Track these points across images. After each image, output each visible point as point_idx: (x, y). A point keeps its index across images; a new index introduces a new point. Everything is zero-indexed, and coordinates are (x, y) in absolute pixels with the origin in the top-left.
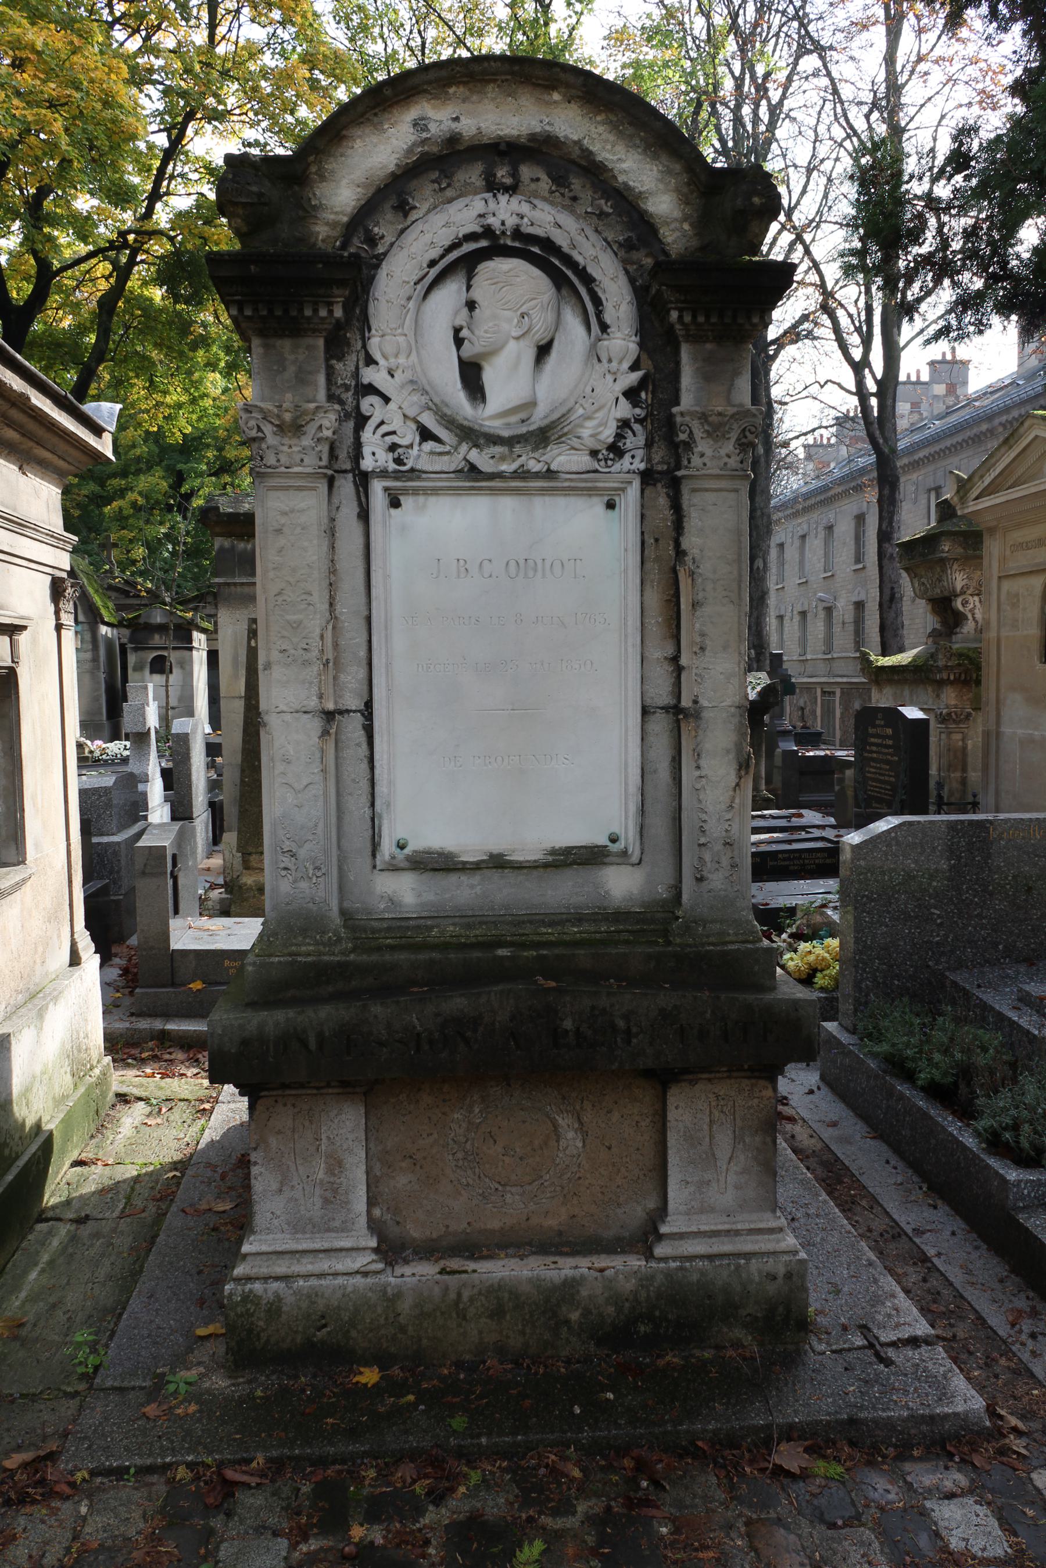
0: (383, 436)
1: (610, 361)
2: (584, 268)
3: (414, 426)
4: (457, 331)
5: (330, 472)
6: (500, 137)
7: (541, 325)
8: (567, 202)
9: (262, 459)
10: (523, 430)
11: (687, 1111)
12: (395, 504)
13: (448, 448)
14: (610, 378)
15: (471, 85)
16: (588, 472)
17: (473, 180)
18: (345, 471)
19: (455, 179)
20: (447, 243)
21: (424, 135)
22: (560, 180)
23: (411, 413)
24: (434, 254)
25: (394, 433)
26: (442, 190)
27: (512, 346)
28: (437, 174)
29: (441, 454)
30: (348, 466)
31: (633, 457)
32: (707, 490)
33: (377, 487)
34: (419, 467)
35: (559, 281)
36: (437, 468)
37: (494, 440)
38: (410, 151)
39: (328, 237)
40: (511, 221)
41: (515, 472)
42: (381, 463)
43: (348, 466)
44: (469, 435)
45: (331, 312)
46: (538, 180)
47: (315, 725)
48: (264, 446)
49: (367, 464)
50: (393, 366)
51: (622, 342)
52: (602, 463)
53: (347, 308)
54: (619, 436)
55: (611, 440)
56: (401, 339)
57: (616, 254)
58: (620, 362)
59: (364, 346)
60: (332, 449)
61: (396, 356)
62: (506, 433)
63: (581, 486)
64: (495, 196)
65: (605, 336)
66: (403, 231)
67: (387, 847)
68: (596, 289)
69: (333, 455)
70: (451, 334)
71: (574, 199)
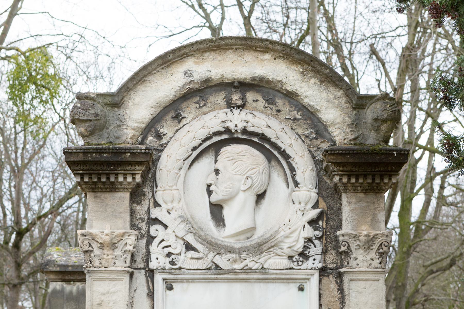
0: (163, 248)
1: (300, 203)
2: (284, 150)
3: (182, 242)
4: (209, 186)
5: (131, 270)
6: (235, 79)
8: (275, 113)
9: (91, 262)
10: (247, 243)
12: (170, 288)
13: (201, 255)
14: (300, 213)
15: (218, 52)
16: (287, 269)
17: (219, 102)
18: (140, 269)
19: (208, 101)
20: (203, 137)
21: (191, 79)
22: (270, 102)
23: (180, 234)
24: (196, 143)
25: (170, 246)
26: (201, 107)
27: (241, 196)
28: (198, 98)
29: (197, 259)
30: (142, 265)
31: (314, 260)
32: (359, 280)
33: (158, 278)
34: (183, 266)
35: (269, 157)
36: (195, 267)
37: (231, 250)
38: (183, 87)
39: (134, 136)
40: (241, 126)
41: (242, 269)
42: (162, 265)
43: (142, 265)
44: (216, 247)
45: (134, 178)
46: (257, 101)
48: (92, 255)
49: (153, 265)
50: (170, 208)
51: (307, 191)
52: (296, 263)
53: (144, 177)
54: (306, 248)
55: (301, 250)
56: (175, 192)
57: (304, 142)
58: (306, 204)
59: (153, 196)
60: (133, 256)
61: (172, 202)
62: (237, 246)
64: (231, 110)
65: (297, 189)
66: (177, 131)
68: (291, 162)
69: (133, 259)
71: (279, 111)
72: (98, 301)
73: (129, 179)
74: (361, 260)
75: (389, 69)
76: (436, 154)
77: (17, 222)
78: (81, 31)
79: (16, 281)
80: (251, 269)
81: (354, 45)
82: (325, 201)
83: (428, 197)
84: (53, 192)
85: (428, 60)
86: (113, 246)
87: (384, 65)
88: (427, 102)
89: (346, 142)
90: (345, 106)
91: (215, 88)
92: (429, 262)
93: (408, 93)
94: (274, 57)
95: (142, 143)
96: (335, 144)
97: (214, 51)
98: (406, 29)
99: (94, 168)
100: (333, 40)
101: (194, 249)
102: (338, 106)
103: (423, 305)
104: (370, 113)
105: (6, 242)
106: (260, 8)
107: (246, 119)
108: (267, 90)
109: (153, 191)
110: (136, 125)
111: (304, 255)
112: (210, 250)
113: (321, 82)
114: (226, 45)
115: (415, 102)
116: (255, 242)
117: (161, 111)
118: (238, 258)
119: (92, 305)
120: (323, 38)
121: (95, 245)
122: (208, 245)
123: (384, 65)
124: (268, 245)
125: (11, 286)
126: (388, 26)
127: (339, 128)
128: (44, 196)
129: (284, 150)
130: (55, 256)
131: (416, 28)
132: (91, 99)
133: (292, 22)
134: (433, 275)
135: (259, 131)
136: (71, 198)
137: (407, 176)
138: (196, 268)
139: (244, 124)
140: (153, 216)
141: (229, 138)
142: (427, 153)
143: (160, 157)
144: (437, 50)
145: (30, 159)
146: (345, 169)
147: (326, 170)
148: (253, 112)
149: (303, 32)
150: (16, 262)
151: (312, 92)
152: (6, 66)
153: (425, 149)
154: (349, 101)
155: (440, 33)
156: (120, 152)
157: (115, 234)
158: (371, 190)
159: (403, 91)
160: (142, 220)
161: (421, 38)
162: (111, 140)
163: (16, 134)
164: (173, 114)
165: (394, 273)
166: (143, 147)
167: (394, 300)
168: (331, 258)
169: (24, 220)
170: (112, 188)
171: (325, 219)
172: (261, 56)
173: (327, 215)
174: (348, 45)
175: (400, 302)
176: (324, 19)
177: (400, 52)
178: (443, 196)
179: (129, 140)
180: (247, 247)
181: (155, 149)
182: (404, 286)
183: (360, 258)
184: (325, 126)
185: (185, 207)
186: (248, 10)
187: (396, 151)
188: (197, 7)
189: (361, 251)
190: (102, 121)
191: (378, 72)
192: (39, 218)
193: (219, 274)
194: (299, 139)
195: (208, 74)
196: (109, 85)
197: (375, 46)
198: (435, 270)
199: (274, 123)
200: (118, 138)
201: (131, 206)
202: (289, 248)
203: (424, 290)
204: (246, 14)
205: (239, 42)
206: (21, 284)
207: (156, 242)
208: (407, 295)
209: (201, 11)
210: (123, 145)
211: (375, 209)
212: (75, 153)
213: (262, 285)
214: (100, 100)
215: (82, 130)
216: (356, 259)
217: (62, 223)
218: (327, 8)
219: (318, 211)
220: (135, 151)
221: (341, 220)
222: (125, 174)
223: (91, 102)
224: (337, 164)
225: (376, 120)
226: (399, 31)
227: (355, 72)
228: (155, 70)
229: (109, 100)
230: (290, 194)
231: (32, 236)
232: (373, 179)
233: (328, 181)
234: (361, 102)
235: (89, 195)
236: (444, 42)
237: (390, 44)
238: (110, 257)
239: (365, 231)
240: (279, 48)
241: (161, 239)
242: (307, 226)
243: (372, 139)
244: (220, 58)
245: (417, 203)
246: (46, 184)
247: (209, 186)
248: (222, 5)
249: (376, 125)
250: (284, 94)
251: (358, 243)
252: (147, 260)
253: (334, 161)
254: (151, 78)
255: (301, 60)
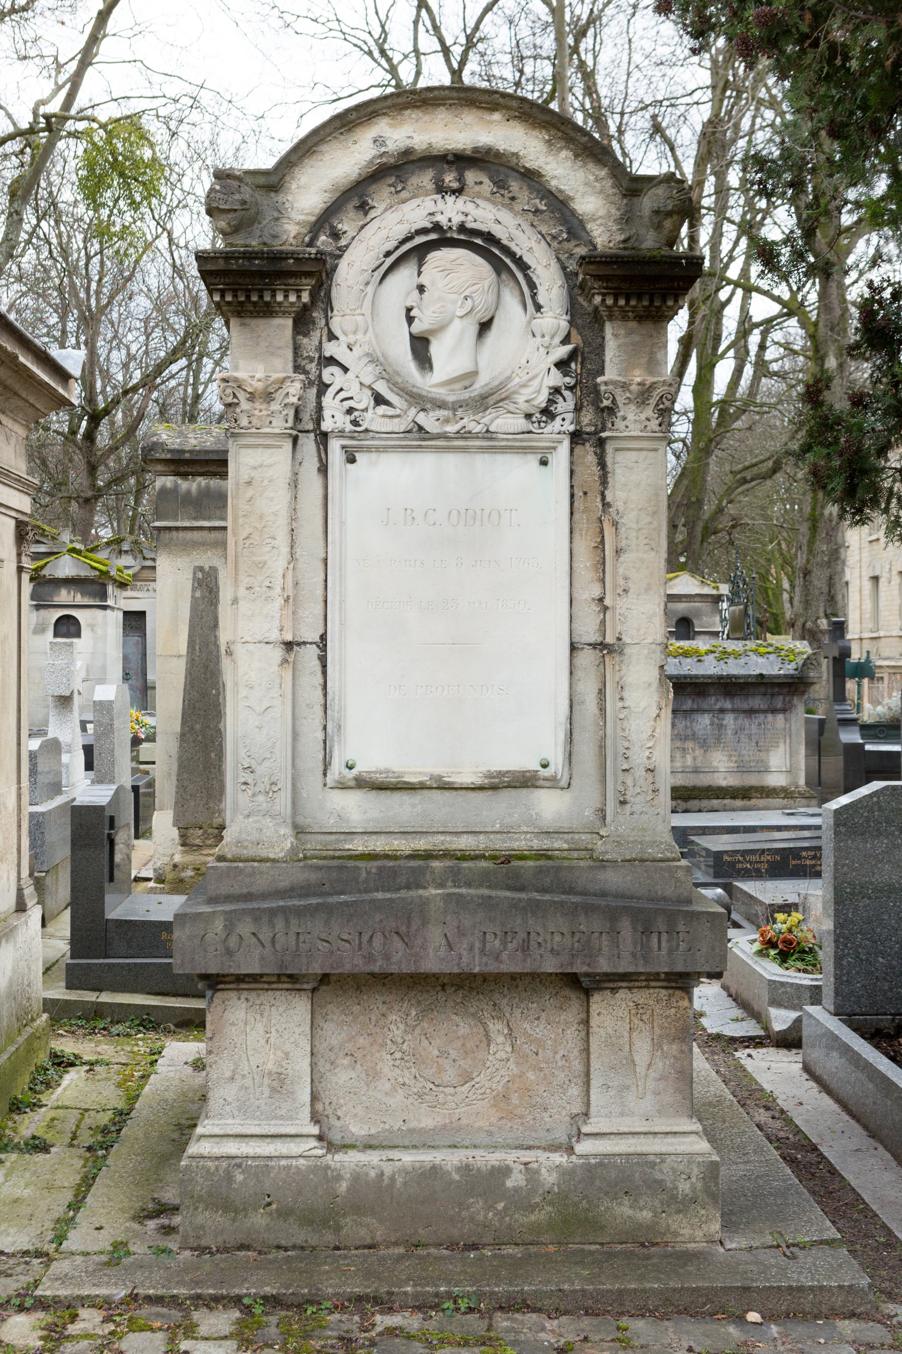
1: (543, 336)
2: (521, 257)
3: (369, 393)
4: (409, 310)
5: (295, 433)
7: (482, 303)
8: (507, 201)
9: (236, 421)
10: (465, 395)
11: (610, 1013)
12: (352, 460)
13: (398, 412)
18: (308, 431)
19: (409, 183)
20: (402, 237)
21: (383, 149)
22: (500, 184)
23: (367, 381)
24: (390, 246)
25: (351, 398)
26: (397, 192)
27: (457, 325)
28: (393, 179)
29: (392, 417)
30: (310, 426)
31: (563, 420)
32: (629, 449)
33: (335, 446)
34: (371, 428)
35: (499, 267)
37: (441, 405)
38: (371, 162)
39: (299, 234)
40: (457, 220)
41: (458, 432)
42: (340, 425)
43: (310, 426)
45: (299, 297)
46: (481, 183)
47: (278, 653)
48: (238, 410)
49: (327, 425)
51: (554, 319)
52: (536, 425)
53: (312, 295)
54: (551, 402)
55: (544, 405)
57: (549, 245)
58: (552, 337)
59: (327, 324)
61: (355, 333)
62: (451, 398)
63: (516, 446)
64: (443, 197)
65: (539, 315)
66: (363, 227)
67: (337, 769)
69: (297, 418)
70: (403, 312)
71: (513, 199)
72: (246, 478)
73: (293, 298)
74: (632, 420)
75: (680, 157)
76: (754, 294)
77: (90, 399)
78: (193, 91)
79: (90, 494)
80: (470, 432)
81: (626, 117)
82: (580, 334)
83: (739, 362)
84: (146, 353)
85: (742, 143)
86: (268, 397)
87: (672, 149)
88: (740, 210)
89: (611, 245)
90: (611, 191)
91: (419, 164)
92: (740, 466)
93: (709, 196)
94: (507, 117)
95: (311, 244)
96: (595, 247)
97: (418, 107)
98: (709, 92)
99: (241, 281)
100: (593, 108)
101: (387, 403)
102: (601, 192)
103: (730, 534)
104: (648, 203)
105: (73, 432)
106: (478, 56)
107: (465, 210)
108: (496, 167)
109: (326, 317)
110: (302, 217)
111: (548, 413)
112: (410, 405)
113: (576, 156)
114: (435, 98)
115: (721, 210)
116: (476, 393)
117: (338, 198)
118: (451, 416)
119: (237, 484)
120: (577, 105)
121: (242, 396)
122: (408, 397)
123: (672, 149)
124: (495, 398)
125: (81, 500)
126: (680, 88)
127: (601, 225)
128: (131, 357)
129: (521, 257)
130: (164, 437)
131: (724, 90)
132: (236, 178)
133: (528, 80)
134: (746, 486)
135: (483, 228)
136: (176, 361)
137: (707, 329)
138: (389, 430)
139: (463, 218)
140: (327, 354)
141: (440, 238)
142: (740, 292)
143: (336, 266)
144: (757, 127)
145: (111, 298)
146: (610, 284)
147: (582, 287)
148: (475, 200)
149: (545, 96)
150: (89, 462)
151: (562, 171)
152: (73, 148)
153: (737, 284)
154: (617, 184)
155: (763, 100)
156: (278, 257)
157: (272, 379)
158: (647, 317)
159: (702, 190)
160: (311, 360)
161: (733, 107)
162: (265, 239)
163: (89, 258)
164: (356, 202)
165: (685, 482)
166: (313, 250)
167: (684, 525)
168: (588, 417)
169: (100, 397)
170: (267, 311)
171: (580, 359)
172: (487, 116)
173: (583, 353)
174: (617, 118)
175: (693, 528)
176: (579, 75)
177: (699, 128)
178: (763, 360)
179: (291, 240)
180: (464, 400)
181: (330, 254)
182: (700, 502)
183: (631, 417)
184: (581, 221)
185: (373, 339)
186: (459, 59)
187: (685, 258)
188: (376, 54)
189: (633, 407)
190: (252, 211)
191: (664, 161)
192: (126, 393)
193: (424, 439)
194: (543, 241)
195: (408, 143)
196: (263, 158)
197: (660, 119)
198: (749, 478)
199: (505, 216)
200: (275, 237)
201: (294, 338)
202: (527, 401)
203: (732, 509)
204: (455, 65)
205: (455, 94)
206: (96, 498)
207: (331, 391)
208: (706, 517)
209: (383, 62)
210: (283, 248)
211: (653, 345)
212: (212, 258)
213: (486, 456)
214: (248, 180)
215: (223, 224)
216: (624, 419)
217: (161, 401)
218: (583, 58)
219: (569, 348)
220: (301, 256)
221: (603, 362)
222: (286, 291)
223: (235, 183)
224: (597, 277)
225: (657, 212)
226: (696, 96)
227: (627, 160)
228: (330, 135)
229: (262, 180)
230: (529, 322)
231: (112, 423)
232: (652, 301)
233: (585, 304)
234: (635, 186)
235: (233, 322)
236: (769, 114)
237: (684, 117)
238: (264, 413)
239: (638, 377)
240: (514, 104)
241: (338, 388)
242: (554, 370)
243: (650, 241)
244: (427, 118)
245: (723, 371)
246: (134, 341)
247: (409, 310)
248: (416, 50)
249: (656, 220)
250: (521, 174)
251: (628, 395)
252: (318, 418)
253: (594, 273)
254: (324, 148)
255: (547, 122)
